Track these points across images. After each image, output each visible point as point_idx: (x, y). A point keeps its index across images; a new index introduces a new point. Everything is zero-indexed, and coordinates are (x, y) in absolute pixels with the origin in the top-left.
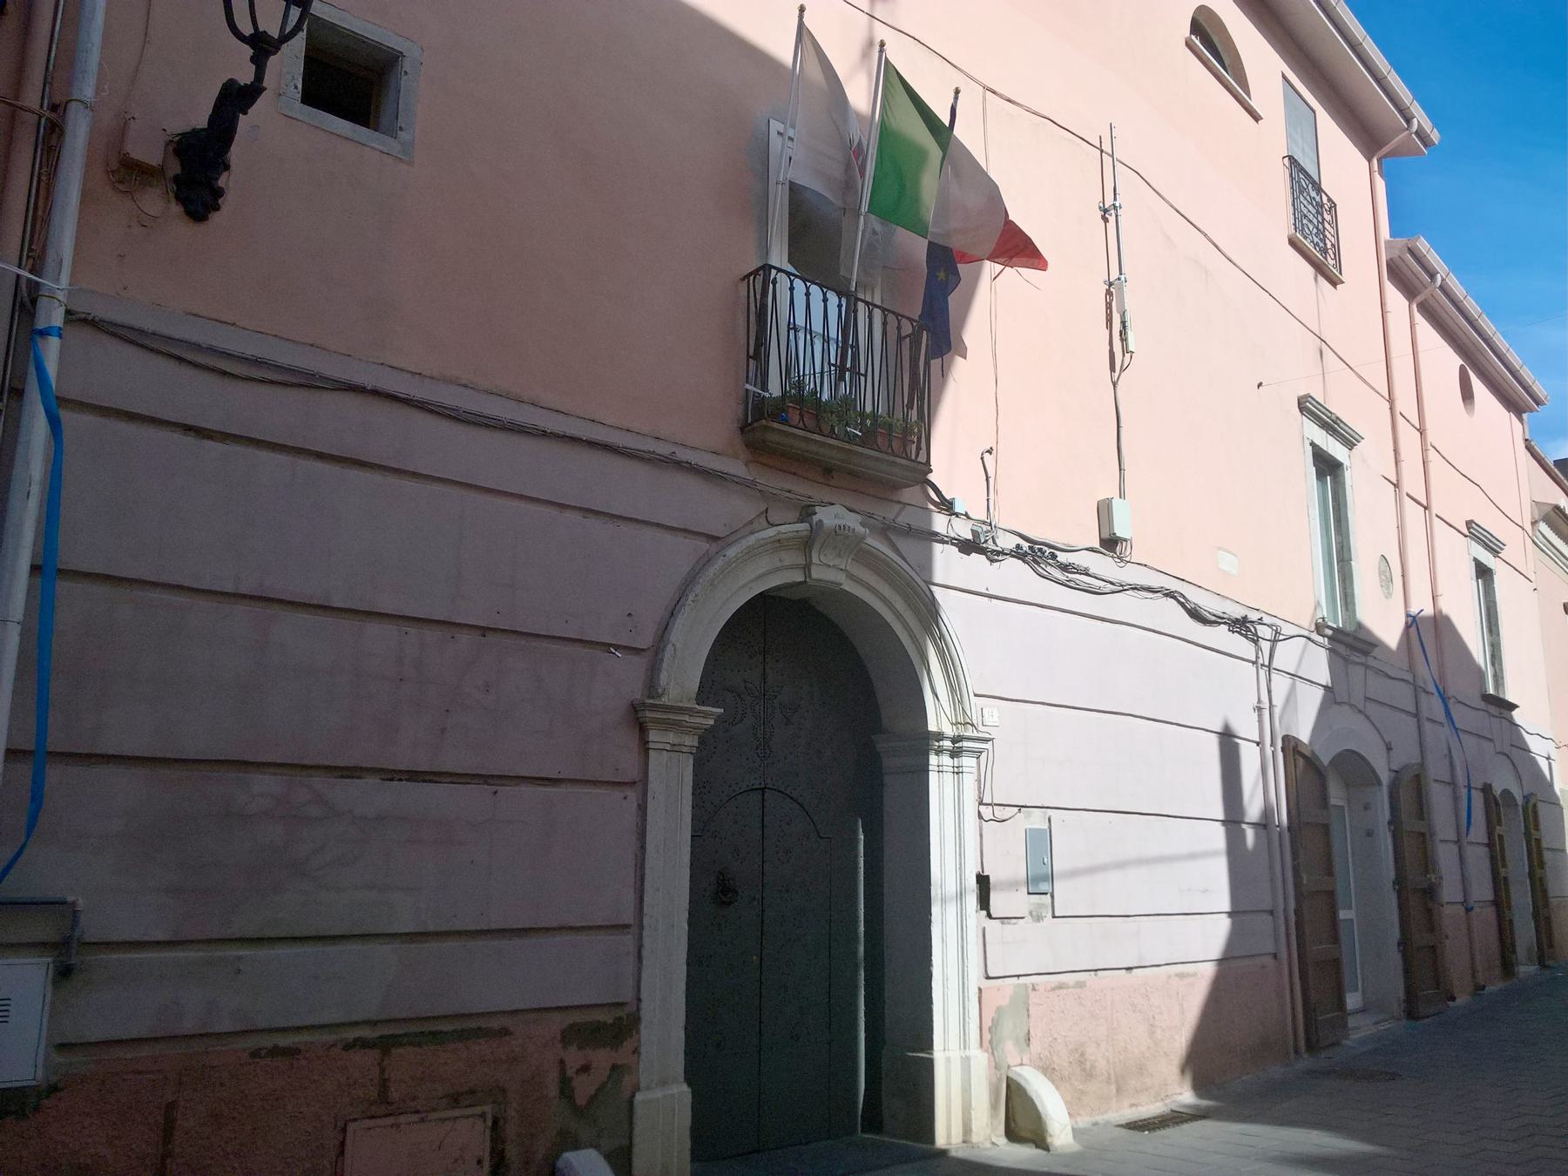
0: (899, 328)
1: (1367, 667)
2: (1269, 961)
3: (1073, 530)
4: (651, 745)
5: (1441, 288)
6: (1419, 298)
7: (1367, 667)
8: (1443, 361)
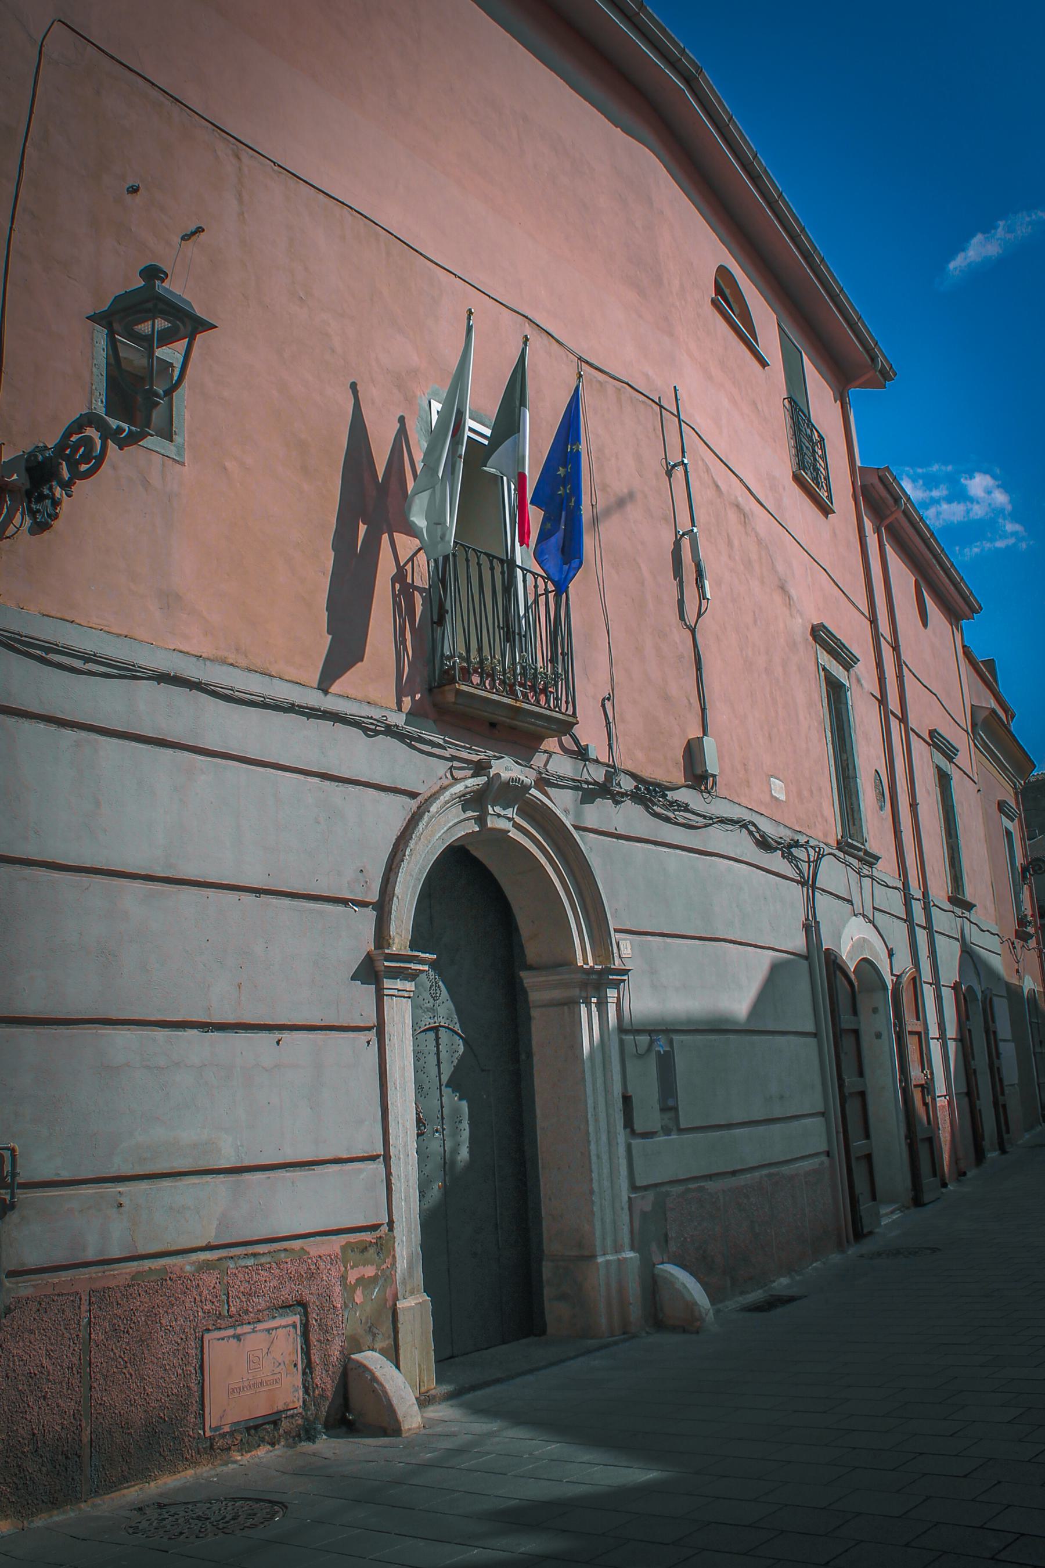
0: (536, 587)
1: (872, 877)
2: (824, 1158)
3: (668, 770)
4: (386, 992)
5: (904, 512)
6: (887, 522)
7: (872, 877)
8: (903, 577)
